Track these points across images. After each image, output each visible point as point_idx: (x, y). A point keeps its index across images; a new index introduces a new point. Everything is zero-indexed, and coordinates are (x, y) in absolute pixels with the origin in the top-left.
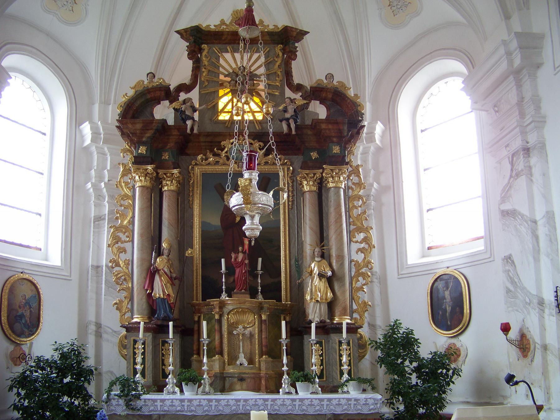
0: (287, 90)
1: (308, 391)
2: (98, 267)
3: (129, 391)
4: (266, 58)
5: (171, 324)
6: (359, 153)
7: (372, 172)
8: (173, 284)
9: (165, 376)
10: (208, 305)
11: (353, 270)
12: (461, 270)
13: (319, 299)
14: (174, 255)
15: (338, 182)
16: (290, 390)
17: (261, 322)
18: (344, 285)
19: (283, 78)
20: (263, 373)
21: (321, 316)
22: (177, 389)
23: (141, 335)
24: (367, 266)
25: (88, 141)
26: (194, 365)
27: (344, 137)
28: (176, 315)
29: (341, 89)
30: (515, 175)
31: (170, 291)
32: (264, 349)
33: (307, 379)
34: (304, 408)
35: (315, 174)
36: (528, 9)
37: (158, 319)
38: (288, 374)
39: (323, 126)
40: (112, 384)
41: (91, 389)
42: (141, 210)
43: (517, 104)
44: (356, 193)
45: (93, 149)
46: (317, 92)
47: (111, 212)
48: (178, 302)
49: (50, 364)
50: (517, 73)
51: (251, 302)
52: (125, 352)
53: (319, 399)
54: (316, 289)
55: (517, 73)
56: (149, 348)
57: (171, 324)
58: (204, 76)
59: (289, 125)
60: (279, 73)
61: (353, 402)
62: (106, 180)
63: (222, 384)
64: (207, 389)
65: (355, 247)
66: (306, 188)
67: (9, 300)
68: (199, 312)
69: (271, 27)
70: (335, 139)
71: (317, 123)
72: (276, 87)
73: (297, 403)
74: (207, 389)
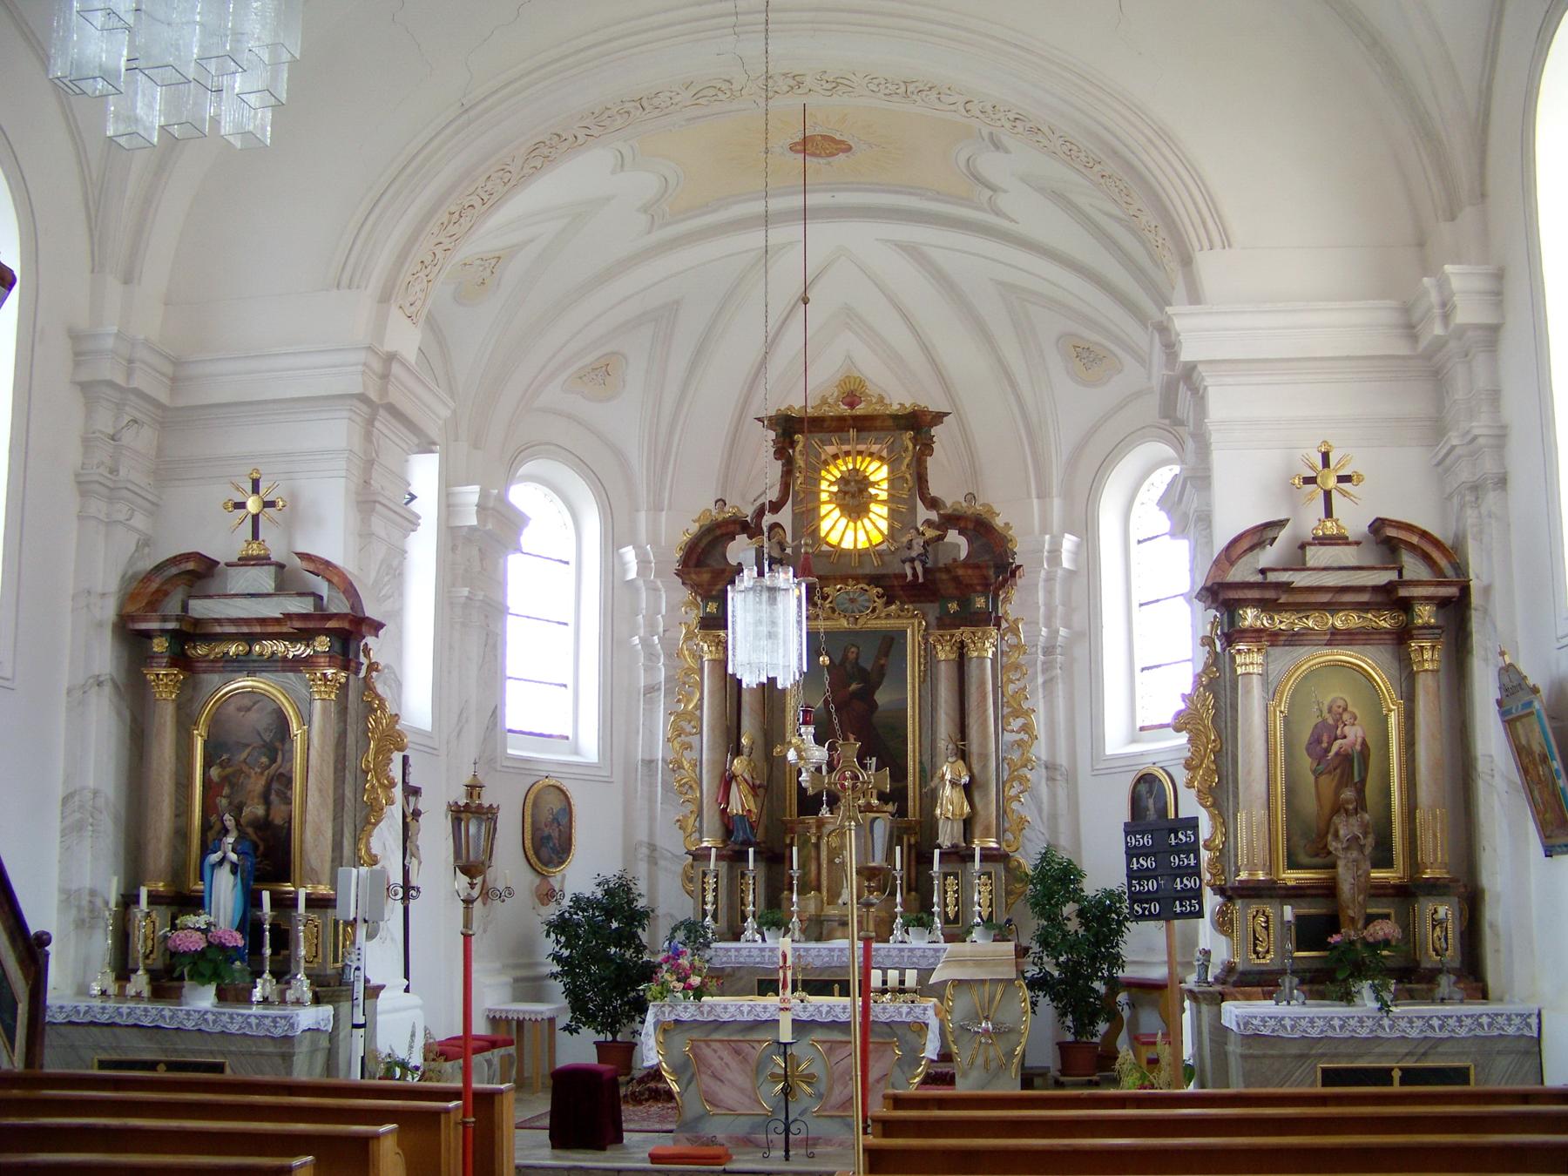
2: (651, 762)
3: (696, 938)
5: (751, 850)
6: (1013, 605)
7: (1060, 609)
8: (755, 795)
9: (744, 919)
10: (803, 822)
12: (1170, 770)
14: (758, 753)
15: (986, 648)
18: (986, 795)
22: (758, 937)
23: (712, 866)
25: (632, 574)
26: (785, 904)
28: (760, 836)
31: (751, 805)
35: (952, 636)
37: (735, 843)
39: (960, 572)
40: (675, 929)
41: (644, 937)
42: (711, 693)
45: (641, 583)
46: (952, 520)
47: (668, 679)
48: (764, 817)
49: (591, 903)
52: (691, 887)
54: (950, 802)
56: (723, 882)
57: (751, 850)
58: (795, 487)
59: (914, 569)
62: (661, 629)
63: (817, 929)
64: (797, 937)
65: (1009, 737)
67: (533, 816)
68: (792, 831)
69: (896, 407)
72: (904, 501)
73: (906, 954)
74: (797, 937)
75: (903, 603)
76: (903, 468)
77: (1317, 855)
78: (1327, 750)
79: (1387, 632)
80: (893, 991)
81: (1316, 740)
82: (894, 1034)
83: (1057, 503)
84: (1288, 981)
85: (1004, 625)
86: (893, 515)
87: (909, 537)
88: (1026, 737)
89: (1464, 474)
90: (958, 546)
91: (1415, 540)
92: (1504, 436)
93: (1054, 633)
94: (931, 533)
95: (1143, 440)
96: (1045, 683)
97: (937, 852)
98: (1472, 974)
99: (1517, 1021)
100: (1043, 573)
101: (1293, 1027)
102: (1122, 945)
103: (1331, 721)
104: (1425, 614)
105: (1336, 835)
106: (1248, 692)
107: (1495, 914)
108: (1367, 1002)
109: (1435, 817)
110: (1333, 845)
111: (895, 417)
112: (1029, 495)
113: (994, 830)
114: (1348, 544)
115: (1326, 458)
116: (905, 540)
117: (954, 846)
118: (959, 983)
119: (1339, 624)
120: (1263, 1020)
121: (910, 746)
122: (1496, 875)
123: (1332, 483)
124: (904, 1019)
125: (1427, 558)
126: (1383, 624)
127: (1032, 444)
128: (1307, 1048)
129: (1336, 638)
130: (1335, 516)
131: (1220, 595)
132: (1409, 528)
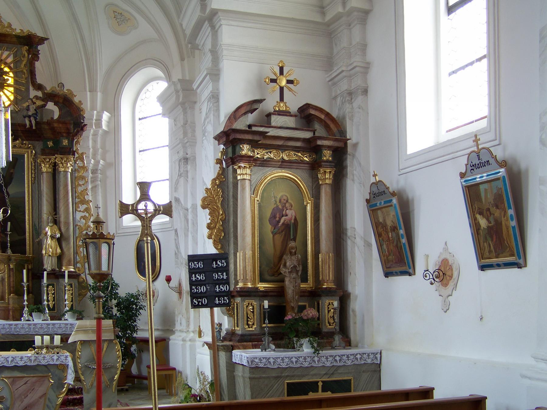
0: (31, 88)
1: (40, 318)
4: (14, 57)
7: (100, 150)
11: (77, 231)
13: (51, 254)
15: (68, 167)
16: (29, 318)
17: (10, 269)
18: (69, 243)
19: (28, 76)
20: (11, 306)
21: (52, 266)
24: (87, 230)
27: (71, 133)
29: (70, 96)
30: (180, 175)
32: (12, 289)
33: (41, 311)
34: (37, 330)
35: (50, 159)
36: (194, 57)
38: (27, 307)
39: (56, 125)
43: (182, 126)
44: (81, 174)
46: (50, 97)
50: (183, 104)
51: (2, 255)
53: (9, 324)
54: (49, 246)
55: (183, 104)
59: (30, 121)
60: (25, 71)
61: (69, 326)
65: (79, 215)
66: (44, 170)
69: (18, 31)
70: (64, 134)
71: (50, 123)
72: (22, 84)
73: (32, 327)
75: (23, 140)
76: (22, 66)
77: (273, 275)
78: (279, 222)
79: (307, 163)
80: (47, 347)
81: (273, 216)
82: (49, 371)
83: (99, 95)
84: (267, 339)
85: (76, 155)
86: (16, 92)
87: (27, 104)
88: (87, 215)
89: (344, 86)
90: (52, 112)
91: (323, 117)
92: (368, 68)
93: (97, 163)
94: (39, 103)
95: (145, 66)
96: (92, 188)
97: (45, 273)
98: (343, 332)
99: (372, 356)
100: (92, 131)
101: (274, 362)
102: (138, 321)
103: (280, 207)
104: (327, 155)
105: (285, 265)
106: (243, 189)
107: (356, 306)
108: (306, 349)
109: (329, 257)
110: (283, 270)
111: (18, 37)
112: (86, 91)
113: (72, 262)
114: (291, 116)
115: (281, 69)
116: (25, 105)
117: (53, 270)
118: (83, 342)
119: (286, 158)
120: (260, 359)
121: (27, 217)
122: (356, 285)
123: (284, 83)
124: (55, 362)
125: (327, 127)
126: (305, 158)
127: (88, 60)
128: (281, 372)
129: (283, 164)
130: (285, 100)
131: (230, 138)
132: (321, 110)
